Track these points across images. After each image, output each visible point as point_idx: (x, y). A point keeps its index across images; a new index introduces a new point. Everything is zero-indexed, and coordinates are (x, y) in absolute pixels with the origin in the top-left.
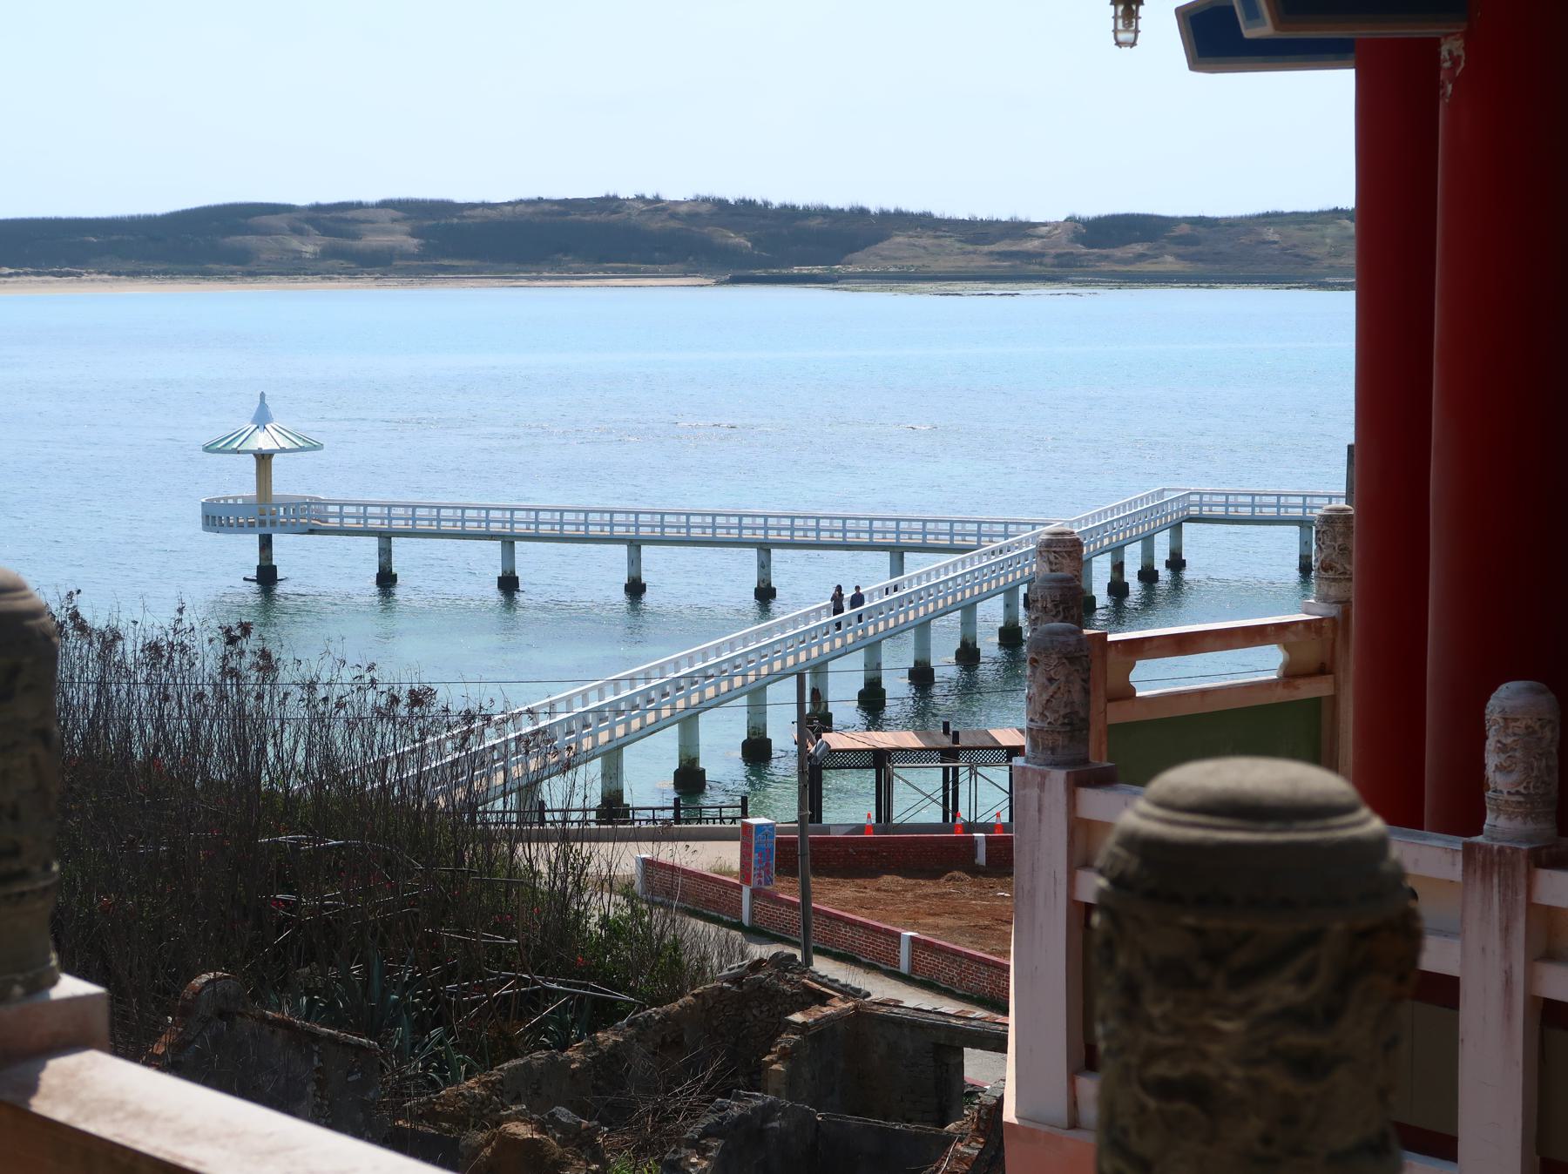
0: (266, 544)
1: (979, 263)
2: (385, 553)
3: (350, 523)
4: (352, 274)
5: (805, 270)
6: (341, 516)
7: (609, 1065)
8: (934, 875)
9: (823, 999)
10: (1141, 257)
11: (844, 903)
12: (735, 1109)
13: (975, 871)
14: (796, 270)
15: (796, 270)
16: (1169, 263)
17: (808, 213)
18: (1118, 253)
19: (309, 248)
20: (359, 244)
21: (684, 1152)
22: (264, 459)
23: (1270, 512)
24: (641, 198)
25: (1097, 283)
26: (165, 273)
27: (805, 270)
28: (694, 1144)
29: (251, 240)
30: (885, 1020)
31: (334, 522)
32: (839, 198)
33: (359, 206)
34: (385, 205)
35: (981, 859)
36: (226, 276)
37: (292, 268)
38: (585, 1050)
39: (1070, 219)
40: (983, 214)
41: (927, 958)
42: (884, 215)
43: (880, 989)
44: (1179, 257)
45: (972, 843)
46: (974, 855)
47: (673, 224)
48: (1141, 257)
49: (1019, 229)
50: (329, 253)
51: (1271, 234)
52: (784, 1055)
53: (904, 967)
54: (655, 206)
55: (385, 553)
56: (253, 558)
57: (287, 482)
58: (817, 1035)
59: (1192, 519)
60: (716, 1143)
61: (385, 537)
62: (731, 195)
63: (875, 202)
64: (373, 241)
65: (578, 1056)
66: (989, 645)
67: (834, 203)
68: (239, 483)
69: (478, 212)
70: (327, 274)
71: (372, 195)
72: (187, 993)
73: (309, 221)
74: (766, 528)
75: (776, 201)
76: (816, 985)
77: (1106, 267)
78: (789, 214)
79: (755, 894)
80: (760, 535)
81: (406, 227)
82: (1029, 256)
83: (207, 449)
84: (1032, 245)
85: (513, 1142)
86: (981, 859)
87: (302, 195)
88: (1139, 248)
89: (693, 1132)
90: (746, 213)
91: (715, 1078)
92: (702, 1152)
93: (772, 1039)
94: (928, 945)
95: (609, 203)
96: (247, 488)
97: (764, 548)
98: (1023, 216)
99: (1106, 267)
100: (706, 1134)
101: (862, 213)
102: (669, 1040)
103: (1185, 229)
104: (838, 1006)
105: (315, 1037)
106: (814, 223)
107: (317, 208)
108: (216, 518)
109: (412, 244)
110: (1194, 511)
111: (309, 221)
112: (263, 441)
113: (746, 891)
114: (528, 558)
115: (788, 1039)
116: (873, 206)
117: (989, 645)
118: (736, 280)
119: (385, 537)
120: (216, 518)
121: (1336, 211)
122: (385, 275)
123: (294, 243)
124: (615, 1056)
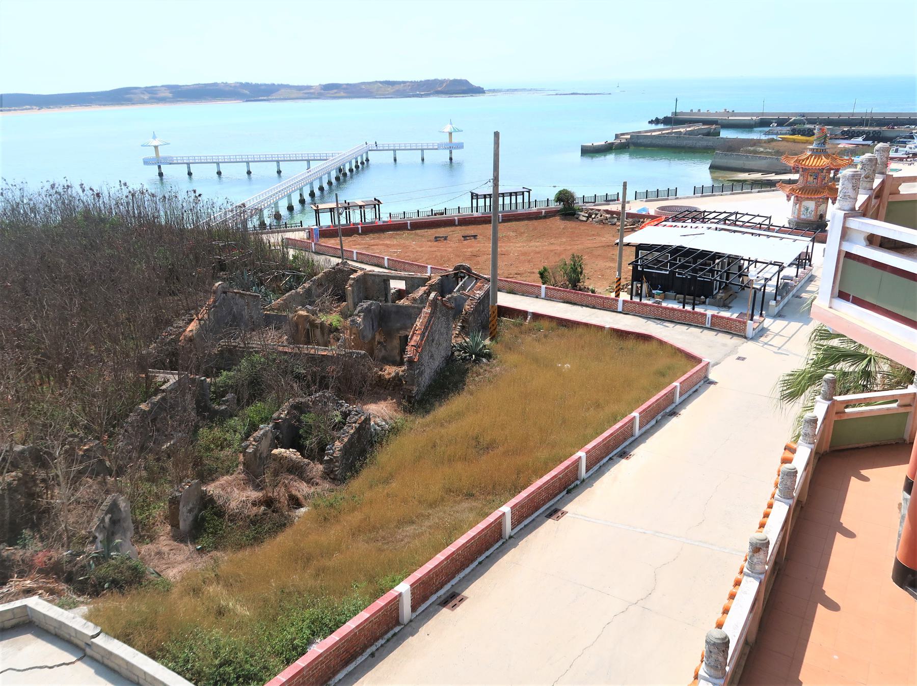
0: (159, 167)
1: (301, 95)
2: (189, 168)
3: (179, 161)
4: (157, 103)
5: (262, 98)
6: (177, 160)
7: (308, 291)
8: (351, 236)
9: (356, 271)
10: (336, 93)
11: (333, 244)
12: (365, 305)
13: (359, 234)
14: (260, 98)
15: (260, 98)
16: (342, 94)
17: (261, 85)
18: (331, 92)
19: (146, 97)
20: (158, 96)
21: (356, 317)
22: (156, 147)
23: (387, 148)
24: (223, 83)
25: (327, 99)
26: (104, 105)
27: (262, 98)
28: (356, 315)
29: (132, 96)
30: (371, 275)
31: (175, 161)
32: (268, 81)
33: (156, 87)
34: (163, 86)
35: (360, 231)
36: (127, 105)
37: (143, 102)
38: (302, 288)
39: (320, 85)
40: (300, 84)
41: (360, 256)
42: (279, 85)
43: (368, 268)
44: (344, 92)
45: (358, 228)
46: (358, 231)
47: (231, 88)
48: (336, 93)
49: (309, 87)
50: (150, 98)
51: (363, 87)
52: (351, 286)
53: (355, 259)
54: (226, 84)
55: (189, 168)
56: (157, 172)
57: (162, 153)
58: (357, 280)
59: (370, 150)
60: (362, 314)
61: (218, 163)
62: (244, 82)
63: (277, 82)
64: (161, 95)
65: (301, 290)
66: (334, 181)
67: (267, 83)
68: (152, 154)
69: (186, 87)
70: (152, 103)
71: (159, 84)
72: (214, 288)
73: (145, 91)
74: (218, 159)
75: (254, 83)
76: (469, 288)
77: (329, 95)
78: (257, 85)
79: (315, 244)
80: (277, 159)
81: (168, 91)
82: (311, 93)
83: (142, 146)
84: (312, 91)
85: (302, 316)
86: (360, 231)
87: (143, 85)
88: (335, 91)
89: (356, 312)
90: (247, 86)
91: (331, 292)
92: (359, 316)
93: (346, 282)
94: (361, 254)
95: (215, 84)
96: (446, 139)
97: (278, 162)
98: (309, 84)
99: (329, 95)
100: (359, 312)
101: (274, 84)
102: (319, 284)
103: (345, 86)
104: (360, 273)
105: (246, 295)
106: (263, 87)
107: (146, 88)
108: (146, 162)
109: (171, 95)
110: (371, 149)
111: (145, 91)
112: (156, 143)
113: (313, 244)
114: (283, 166)
115: (351, 282)
116: (276, 83)
117: (334, 181)
118: (247, 101)
119: (188, 164)
120: (146, 162)
121: (376, 81)
122: (165, 103)
123: (142, 96)
124: (309, 289)
